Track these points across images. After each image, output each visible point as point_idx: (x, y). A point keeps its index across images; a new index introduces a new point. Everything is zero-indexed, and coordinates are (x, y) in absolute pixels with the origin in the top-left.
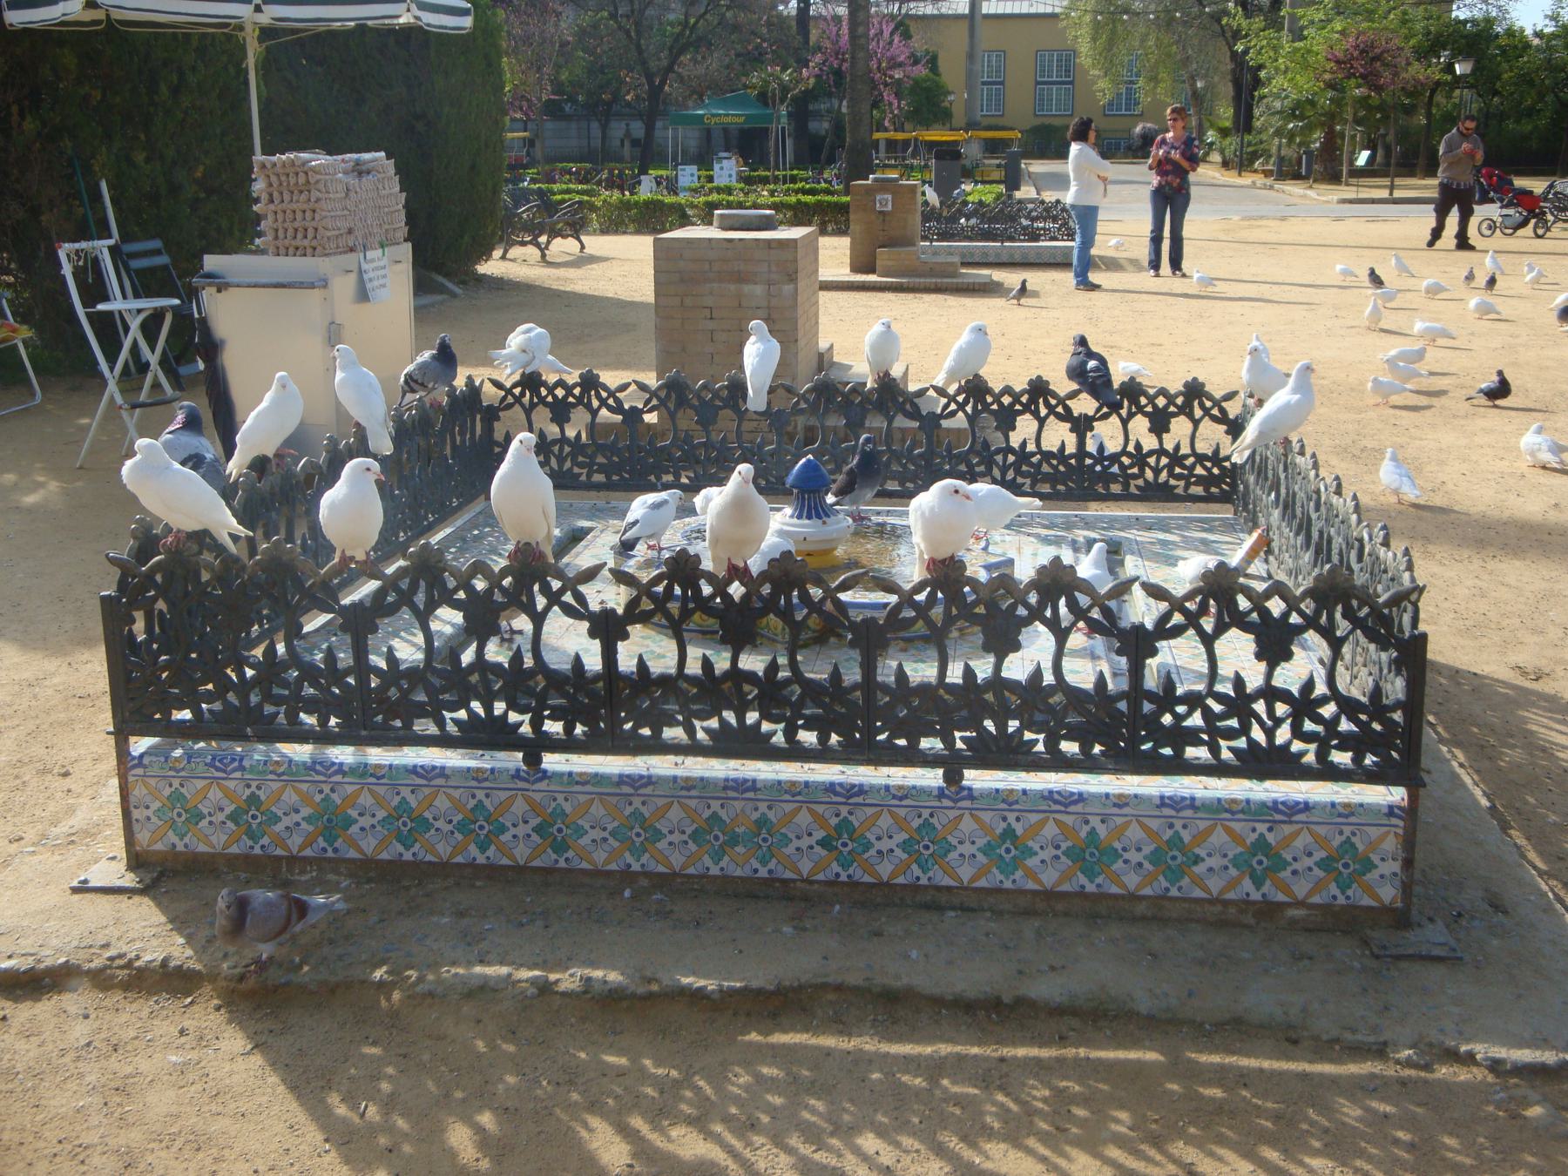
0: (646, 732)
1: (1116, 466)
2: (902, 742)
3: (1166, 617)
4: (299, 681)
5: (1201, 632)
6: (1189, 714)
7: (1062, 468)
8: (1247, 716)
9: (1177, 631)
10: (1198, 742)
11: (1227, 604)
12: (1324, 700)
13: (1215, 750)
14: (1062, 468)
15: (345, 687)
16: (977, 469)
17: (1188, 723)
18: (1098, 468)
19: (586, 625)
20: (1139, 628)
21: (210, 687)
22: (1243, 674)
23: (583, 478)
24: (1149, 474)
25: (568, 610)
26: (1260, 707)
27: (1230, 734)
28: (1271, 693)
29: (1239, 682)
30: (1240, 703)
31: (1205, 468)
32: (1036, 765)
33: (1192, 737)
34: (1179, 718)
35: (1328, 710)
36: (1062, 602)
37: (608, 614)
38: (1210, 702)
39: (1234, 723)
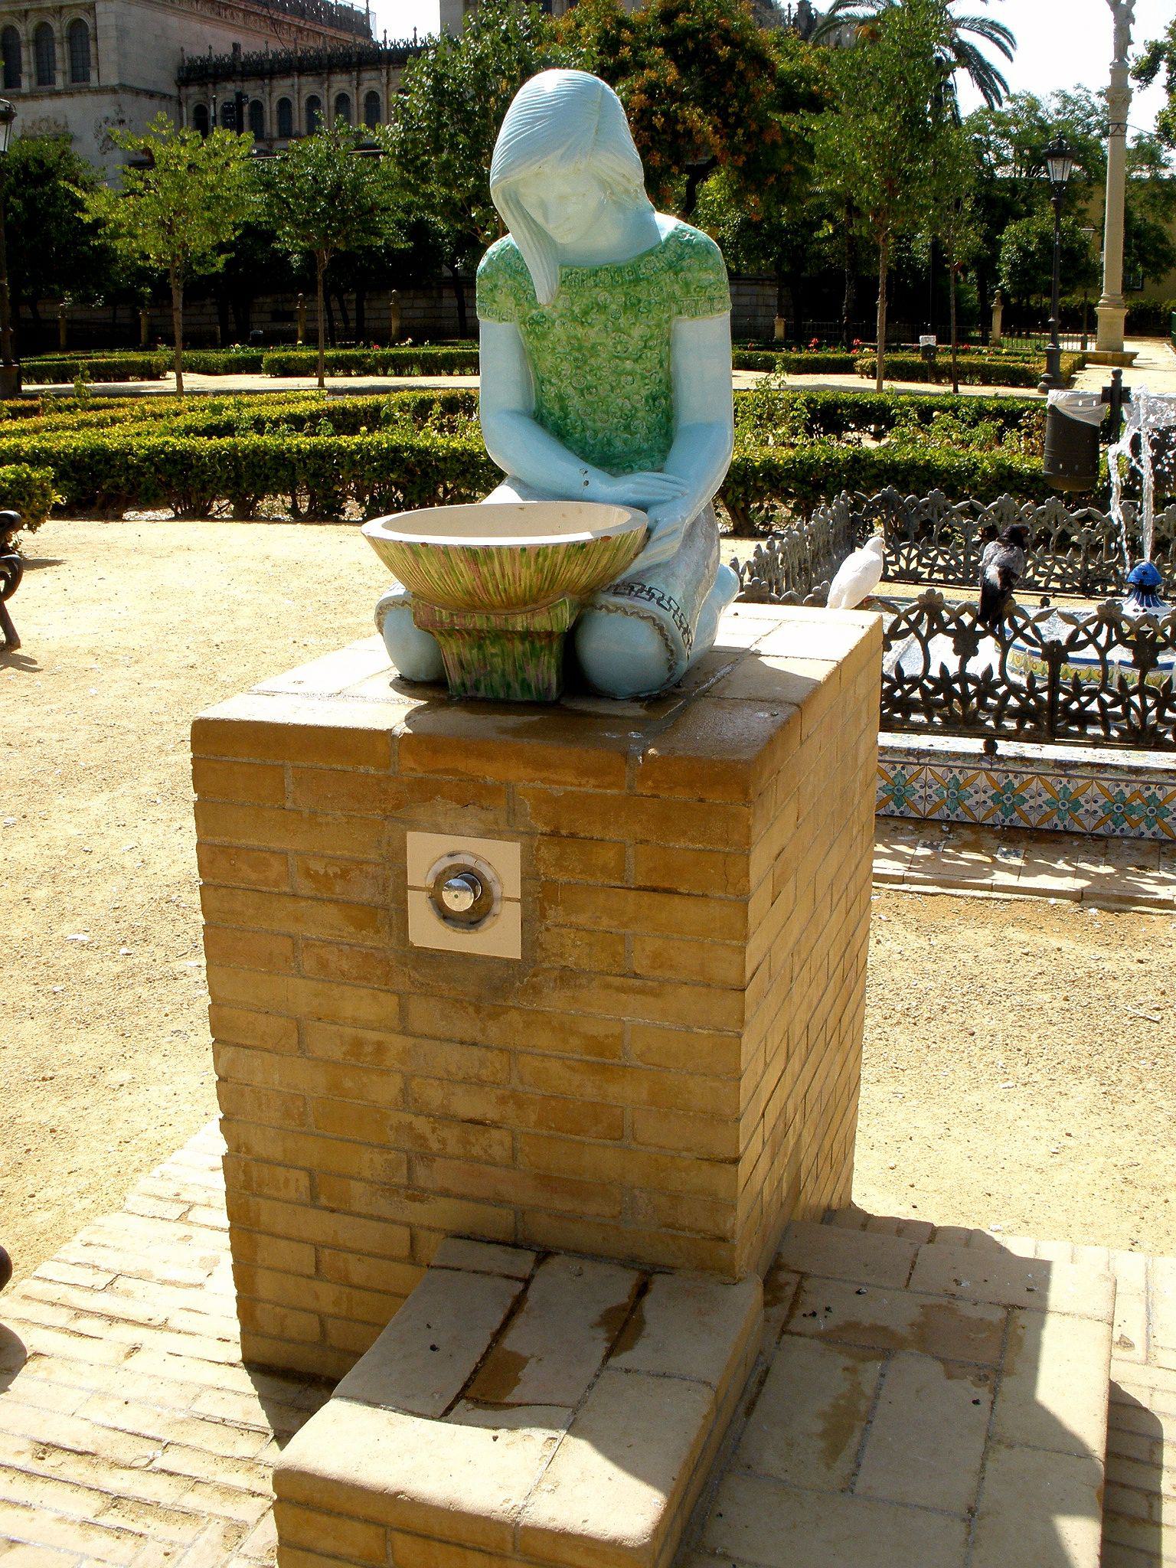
0: (898, 715)
2: (1076, 729)
3: (1074, 635)
4: (1006, 696)
5: (919, 635)
9: (904, 634)
11: (935, 617)
12: (999, 684)
15: (1039, 700)
16: (888, 559)
18: (898, 693)
21: (941, 697)
26: (1136, 699)
27: (892, 563)
29: (943, 669)
30: (944, 681)
34: (1083, 705)
35: (1001, 690)
38: (925, 682)
39: (1119, 709)
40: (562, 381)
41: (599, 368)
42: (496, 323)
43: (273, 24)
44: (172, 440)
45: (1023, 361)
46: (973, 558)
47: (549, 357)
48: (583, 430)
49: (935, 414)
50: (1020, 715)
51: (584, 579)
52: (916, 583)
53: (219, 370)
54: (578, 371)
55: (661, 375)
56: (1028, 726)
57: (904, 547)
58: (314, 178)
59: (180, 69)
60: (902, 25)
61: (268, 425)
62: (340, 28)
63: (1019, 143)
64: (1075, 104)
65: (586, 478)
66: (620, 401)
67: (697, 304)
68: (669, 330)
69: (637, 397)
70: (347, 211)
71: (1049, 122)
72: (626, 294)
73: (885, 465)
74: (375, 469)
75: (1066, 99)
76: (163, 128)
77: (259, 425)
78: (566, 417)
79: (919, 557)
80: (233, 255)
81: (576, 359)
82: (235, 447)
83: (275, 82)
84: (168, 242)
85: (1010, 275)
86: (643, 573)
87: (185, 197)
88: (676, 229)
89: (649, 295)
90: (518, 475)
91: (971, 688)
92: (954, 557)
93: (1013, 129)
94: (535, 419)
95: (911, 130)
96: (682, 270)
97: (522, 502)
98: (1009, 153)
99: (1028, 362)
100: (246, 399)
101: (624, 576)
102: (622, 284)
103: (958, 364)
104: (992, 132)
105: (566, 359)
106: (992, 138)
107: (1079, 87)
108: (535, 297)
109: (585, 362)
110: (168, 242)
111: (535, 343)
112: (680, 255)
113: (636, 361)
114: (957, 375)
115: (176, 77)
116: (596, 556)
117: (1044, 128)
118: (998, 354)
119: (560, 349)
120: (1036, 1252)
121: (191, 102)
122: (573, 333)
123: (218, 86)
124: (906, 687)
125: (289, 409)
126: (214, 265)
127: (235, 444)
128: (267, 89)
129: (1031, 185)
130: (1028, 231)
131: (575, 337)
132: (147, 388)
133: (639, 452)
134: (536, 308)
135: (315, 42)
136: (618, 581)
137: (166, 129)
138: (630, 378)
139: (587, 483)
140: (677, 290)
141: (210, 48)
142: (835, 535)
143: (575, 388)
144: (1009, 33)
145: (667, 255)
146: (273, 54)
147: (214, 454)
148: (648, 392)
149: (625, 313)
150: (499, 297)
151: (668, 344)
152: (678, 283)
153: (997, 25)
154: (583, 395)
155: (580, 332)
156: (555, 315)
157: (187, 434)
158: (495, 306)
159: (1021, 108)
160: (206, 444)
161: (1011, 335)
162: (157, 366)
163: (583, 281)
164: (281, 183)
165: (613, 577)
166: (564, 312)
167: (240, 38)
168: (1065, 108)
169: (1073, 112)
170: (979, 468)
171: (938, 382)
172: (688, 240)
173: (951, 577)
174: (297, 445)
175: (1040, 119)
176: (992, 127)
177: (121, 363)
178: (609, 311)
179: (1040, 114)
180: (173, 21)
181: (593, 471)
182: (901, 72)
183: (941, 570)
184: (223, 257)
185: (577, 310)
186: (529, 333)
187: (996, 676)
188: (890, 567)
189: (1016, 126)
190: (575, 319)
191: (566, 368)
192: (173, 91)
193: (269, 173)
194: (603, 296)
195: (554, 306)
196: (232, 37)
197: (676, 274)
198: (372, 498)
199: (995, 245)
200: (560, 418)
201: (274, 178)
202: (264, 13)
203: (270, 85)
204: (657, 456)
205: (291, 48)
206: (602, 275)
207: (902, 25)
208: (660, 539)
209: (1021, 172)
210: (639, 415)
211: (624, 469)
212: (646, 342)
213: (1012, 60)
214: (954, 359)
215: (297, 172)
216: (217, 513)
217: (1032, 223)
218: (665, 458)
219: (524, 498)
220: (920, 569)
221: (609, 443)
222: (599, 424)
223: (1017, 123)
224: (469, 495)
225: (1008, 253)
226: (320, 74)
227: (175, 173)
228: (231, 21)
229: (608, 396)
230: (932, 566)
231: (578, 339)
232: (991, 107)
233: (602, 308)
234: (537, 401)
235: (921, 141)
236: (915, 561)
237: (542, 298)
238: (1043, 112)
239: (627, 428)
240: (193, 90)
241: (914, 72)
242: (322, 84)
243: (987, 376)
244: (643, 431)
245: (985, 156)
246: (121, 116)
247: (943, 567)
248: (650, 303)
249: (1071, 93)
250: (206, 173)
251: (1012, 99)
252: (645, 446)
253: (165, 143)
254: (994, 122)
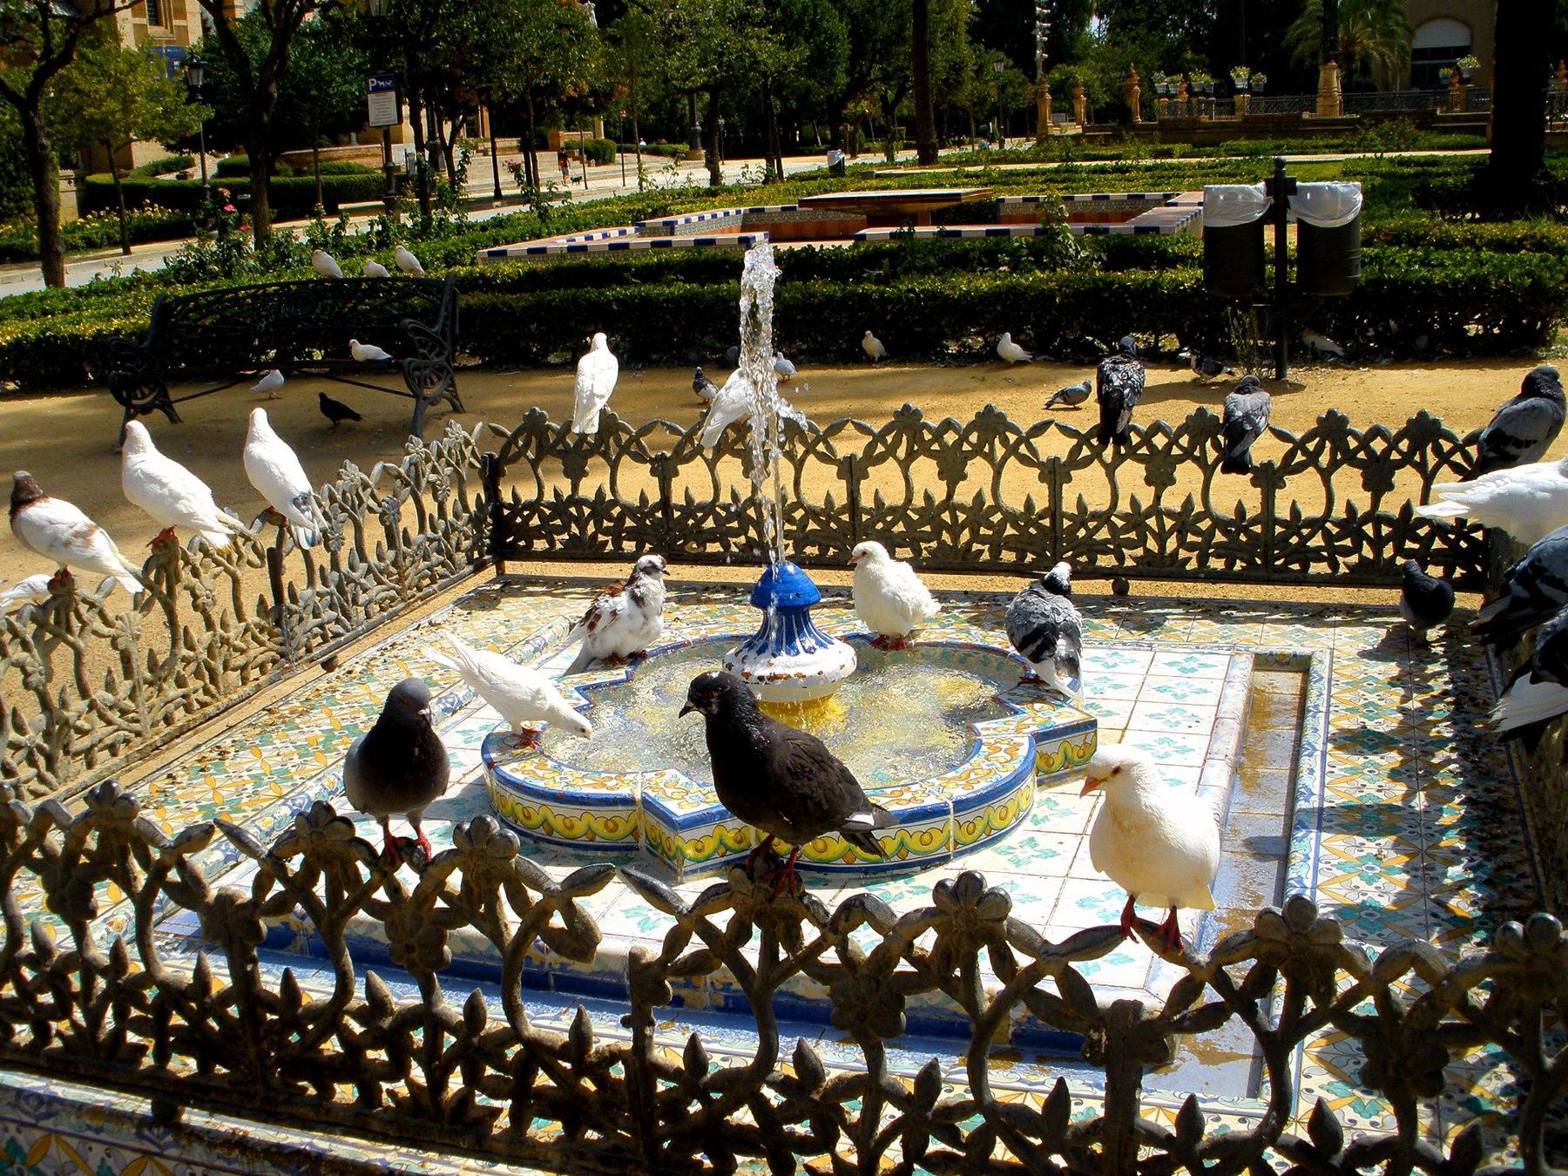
0: (1295, 567)
2: (1295, 567)
4: (1002, 524)
6: (1311, 536)
8: (1359, 537)
9: (881, 459)
10: (1106, 552)
11: (916, 437)
12: (1200, 517)
13: (1334, 566)
15: (1040, 528)
17: (1311, 544)
18: (1294, 540)
19: (1037, 471)
20: (1269, 465)
22: (1033, 498)
23: (610, 547)
25: (1024, 460)
27: (1347, 552)
28: (1373, 517)
30: (930, 512)
32: (1193, 577)
34: (1091, 533)
35: (1205, 525)
36: (1208, 443)
37: (851, 459)
39: (1348, 542)
50: (638, 535)
56: (832, 551)
91: (587, 511)
124: (1091, 525)
187: (792, 499)
220: (1183, 554)
224: (168, 284)
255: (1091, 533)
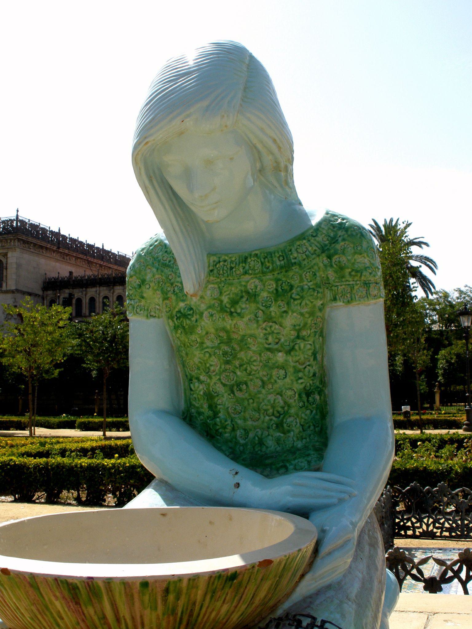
1: (410, 522)
7: (454, 525)
9: (450, 579)
14: (454, 525)
16: (416, 525)
17: (407, 525)
18: (402, 523)
24: (424, 527)
25: (414, 577)
27: (418, 528)
31: (449, 524)
33: (408, 528)
40: (210, 378)
41: (249, 362)
42: (144, 319)
43: (89, 263)
44: (14, 458)
45: (453, 416)
46: (466, 522)
47: (197, 353)
48: (233, 429)
49: (419, 443)
51: (235, 618)
52: (433, 539)
53: (55, 427)
54: (228, 367)
55: (315, 368)
57: (425, 518)
58: (103, 332)
59: (44, 282)
60: (389, 250)
61: (67, 453)
62: (120, 266)
63: (441, 314)
64: (465, 294)
65: (237, 479)
66: (271, 397)
67: (352, 288)
68: (323, 318)
69: (289, 393)
70: (119, 348)
71: (454, 303)
72: (277, 280)
73: (401, 471)
74: (121, 477)
75: (461, 292)
76: (28, 303)
77: (63, 453)
78: (216, 415)
79: (434, 523)
80: (62, 369)
81: (225, 354)
82: (47, 463)
83: (88, 290)
84: (28, 360)
85: (443, 375)
86: (310, 599)
87: (37, 337)
88: (327, 213)
89: (301, 280)
90: (165, 478)
92: (455, 521)
93: (437, 307)
94: (184, 419)
95: (396, 301)
96: (336, 253)
97: (165, 507)
98: (436, 318)
99: (456, 417)
100: (61, 440)
101: (287, 605)
102: (273, 270)
103: (421, 419)
104: (428, 309)
105: (215, 354)
106: (428, 311)
107: (466, 286)
108: (182, 289)
109: (235, 357)
110: (28, 360)
111: (183, 338)
112: (333, 238)
113: (288, 352)
114: (421, 425)
115: (42, 286)
116: (252, 588)
117: (452, 306)
118: (439, 414)
119: (208, 343)
120: (103, 246)
121: (48, 298)
122: (220, 324)
123: (61, 291)
125: (81, 445)
126: (53, 374)
127: (47, 462)
128: (84, 293)
129: (448, 332)
130: (450, 353)
131: (224, 329)
132: (18, 434)
133: (293, 451)
134: (183, 301)
135: (108, 271)
136: (280, 612)
137: (29, 304)
138: (282, 372)
139: (238, 485)
140: (331, 274)
141: (59, 273)
142: (386, 513)
143: (224, 385)
144: (434, 262)
145: (319, 238)
146: (88, 276)
147: (36, 467)
148: (302, 386)
149: (276, 300)
150: (148, 293)
151: (321, 334)
152: (331, 266)
153: (428, 258)
154: (233, 392)
155: (229, 323)
156: (203, 307)
157: (23, 456)
158: (143, 303)
159: (441, 297)
160: (32, 461)
161: (443, 406)
162: (24, 423)
163: (232, 268)
164: (87, 334)
165: (274, 608)
166: (213, 302)
167: (73, 269)
168: (461, 296)
169: (464, 298)
170: (453, 470)
171: (412, 429)
172: (340, 224)
173: (453, 534)
174: (81, 464)
175: (450, 302)
176: (428, 306)
177: (6, 421)
178: (260, 299)
179: (449, 299)
180: (42, 261)
181: (244, 471)
182: (390, 273)
183: (448, 530)
184: (58, 370)
185: (225, 299)
186: (176, 328)
188: (417, 530)
189: (439, 305)
190: (223, 309)
191: (215, 363)
192: (40, 293)
193: (81, 329)
194: (252, 283)
195: (202, 297)
196: (68, 268)
197: (329, 257)
198: (120, 493)
199: (434, 361)
200: (208, 417)
201: (83, 332)
202: (84, 258)
203: (86, 291)
204: (314, 455)
205: (96, 274)
206: (252, 262)
207: (389, 250)
208: (329, 554)
209: (442, 327)
210: (292, 411)
211: (278, 470)
212: (299, 331)
213: (435, 274)
214: (420, 417)
215: (95, 329)
216: (38, 499)
217: (452, 349)
218: (321, 457)
219: (168, 505)
220: (435, 530)
221: (261, 443)
222: (250, 423)
223: (439, 304)
225: (442, 364)
226: (110, 286)
227: (33, 326)
228: (69, 261)
229: (260, 392)
230: (441, 528)
231: (227, 332)
232: (427, 297)
233: (252, 296)
234: (186, 401)
235: (402, 306)
236: (432, 525)
237: (189, 287)
238: (451, 298)
239: (279, 426)
240: (50, 292)
241: (397, 273)
242: (110, 290)
243: (437, 425)
244: (297, 429)
245: (426, 320)
246: (15, 304)
247: (449, 528)
248: (302, 289)
249: (464, 289)
250: (48, 326)
251: (436, 293)
252: (299, 444)
253: (29, 311)
254: (429, 304)
255: (405, 523)
